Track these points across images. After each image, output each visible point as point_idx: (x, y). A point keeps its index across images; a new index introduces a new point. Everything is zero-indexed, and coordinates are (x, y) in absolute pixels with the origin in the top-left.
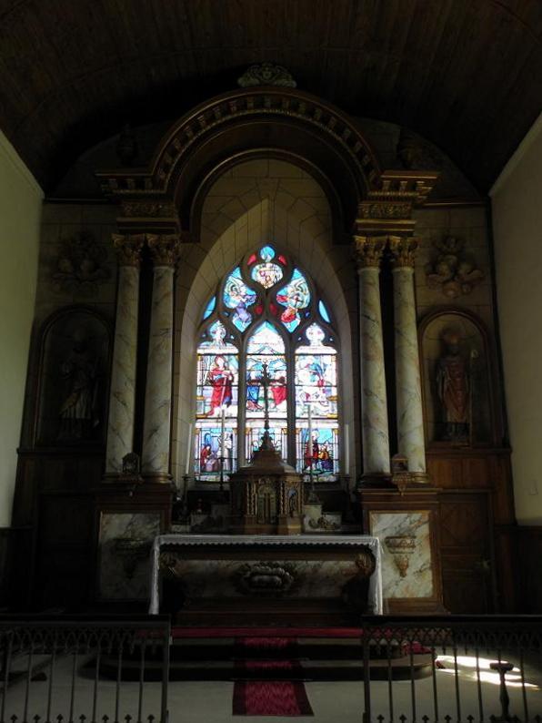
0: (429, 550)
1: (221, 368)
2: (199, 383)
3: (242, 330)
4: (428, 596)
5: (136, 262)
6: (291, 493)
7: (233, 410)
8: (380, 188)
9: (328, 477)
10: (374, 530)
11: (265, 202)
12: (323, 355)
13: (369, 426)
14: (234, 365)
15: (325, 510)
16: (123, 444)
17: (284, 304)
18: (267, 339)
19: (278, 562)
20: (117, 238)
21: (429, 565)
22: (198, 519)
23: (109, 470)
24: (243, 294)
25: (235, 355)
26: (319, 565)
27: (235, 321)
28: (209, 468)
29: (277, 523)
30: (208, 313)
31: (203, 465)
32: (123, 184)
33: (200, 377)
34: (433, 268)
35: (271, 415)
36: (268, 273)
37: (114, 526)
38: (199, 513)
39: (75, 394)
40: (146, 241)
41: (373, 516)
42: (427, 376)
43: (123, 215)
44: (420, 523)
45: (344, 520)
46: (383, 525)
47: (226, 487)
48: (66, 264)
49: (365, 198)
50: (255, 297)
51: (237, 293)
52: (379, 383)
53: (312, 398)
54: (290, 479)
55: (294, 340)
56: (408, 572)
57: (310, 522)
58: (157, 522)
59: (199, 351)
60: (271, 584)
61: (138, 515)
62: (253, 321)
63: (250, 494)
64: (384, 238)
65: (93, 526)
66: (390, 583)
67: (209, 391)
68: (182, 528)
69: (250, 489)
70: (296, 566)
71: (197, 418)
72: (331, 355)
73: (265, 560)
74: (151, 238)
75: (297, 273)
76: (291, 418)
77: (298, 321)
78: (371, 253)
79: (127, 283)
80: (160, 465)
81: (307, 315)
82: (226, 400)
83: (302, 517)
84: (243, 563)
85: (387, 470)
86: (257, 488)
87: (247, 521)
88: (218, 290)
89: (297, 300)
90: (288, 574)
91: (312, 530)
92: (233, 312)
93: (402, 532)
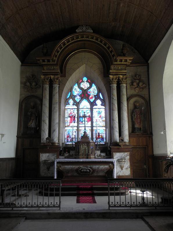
1: (72, 112)
2: (66, 117)
5: (48, 83)
7: (76, 124)
9: (102, 143)
10: (114, 157)
13: (113, 129)
14: (76, 111)
15: (101, 152)
16: (45, 135)
17: (90, 94)
18: (85, 104)
20: (42, 77)
21: (129, 167)
22: (67, 155)
23: (42, 141)
24: (78, 91)
25: (76, 109)
27: (76, 99)
28: (69, 141)
29: (88, 156)
30: (68, 97)
31: (67, 139)
32: (44, 61)
33: (66, 115)
34: (132, 84)
36: (85, 85)
37: (44, 157)
40: (51, 77)
41: (114, 154)
42: (130, 115)
45: (106, 155)
46: (117, 156)
47: (74, 146)
48: (28, 84)
49: (112, 64)
51: (76, 91)
52: (116, 117)
54: (91, 144)
55: (93, 104)
56: (123, 168)
58: (55, 156)
59: (66, 108)
60: (86, 172)
61: (50, 154)
62: (81, 99)
65: (38, 157)
67: (69, 119)
74: (52, 77)
75: (93, 84)
76: (92, 126)
77: (94, 99)
79: (46, 89)
80: (56, 140)
83: (95, 154)
84: (79, 166)
85: (118, 141)
87: (80, 155)
88: (71, 90)
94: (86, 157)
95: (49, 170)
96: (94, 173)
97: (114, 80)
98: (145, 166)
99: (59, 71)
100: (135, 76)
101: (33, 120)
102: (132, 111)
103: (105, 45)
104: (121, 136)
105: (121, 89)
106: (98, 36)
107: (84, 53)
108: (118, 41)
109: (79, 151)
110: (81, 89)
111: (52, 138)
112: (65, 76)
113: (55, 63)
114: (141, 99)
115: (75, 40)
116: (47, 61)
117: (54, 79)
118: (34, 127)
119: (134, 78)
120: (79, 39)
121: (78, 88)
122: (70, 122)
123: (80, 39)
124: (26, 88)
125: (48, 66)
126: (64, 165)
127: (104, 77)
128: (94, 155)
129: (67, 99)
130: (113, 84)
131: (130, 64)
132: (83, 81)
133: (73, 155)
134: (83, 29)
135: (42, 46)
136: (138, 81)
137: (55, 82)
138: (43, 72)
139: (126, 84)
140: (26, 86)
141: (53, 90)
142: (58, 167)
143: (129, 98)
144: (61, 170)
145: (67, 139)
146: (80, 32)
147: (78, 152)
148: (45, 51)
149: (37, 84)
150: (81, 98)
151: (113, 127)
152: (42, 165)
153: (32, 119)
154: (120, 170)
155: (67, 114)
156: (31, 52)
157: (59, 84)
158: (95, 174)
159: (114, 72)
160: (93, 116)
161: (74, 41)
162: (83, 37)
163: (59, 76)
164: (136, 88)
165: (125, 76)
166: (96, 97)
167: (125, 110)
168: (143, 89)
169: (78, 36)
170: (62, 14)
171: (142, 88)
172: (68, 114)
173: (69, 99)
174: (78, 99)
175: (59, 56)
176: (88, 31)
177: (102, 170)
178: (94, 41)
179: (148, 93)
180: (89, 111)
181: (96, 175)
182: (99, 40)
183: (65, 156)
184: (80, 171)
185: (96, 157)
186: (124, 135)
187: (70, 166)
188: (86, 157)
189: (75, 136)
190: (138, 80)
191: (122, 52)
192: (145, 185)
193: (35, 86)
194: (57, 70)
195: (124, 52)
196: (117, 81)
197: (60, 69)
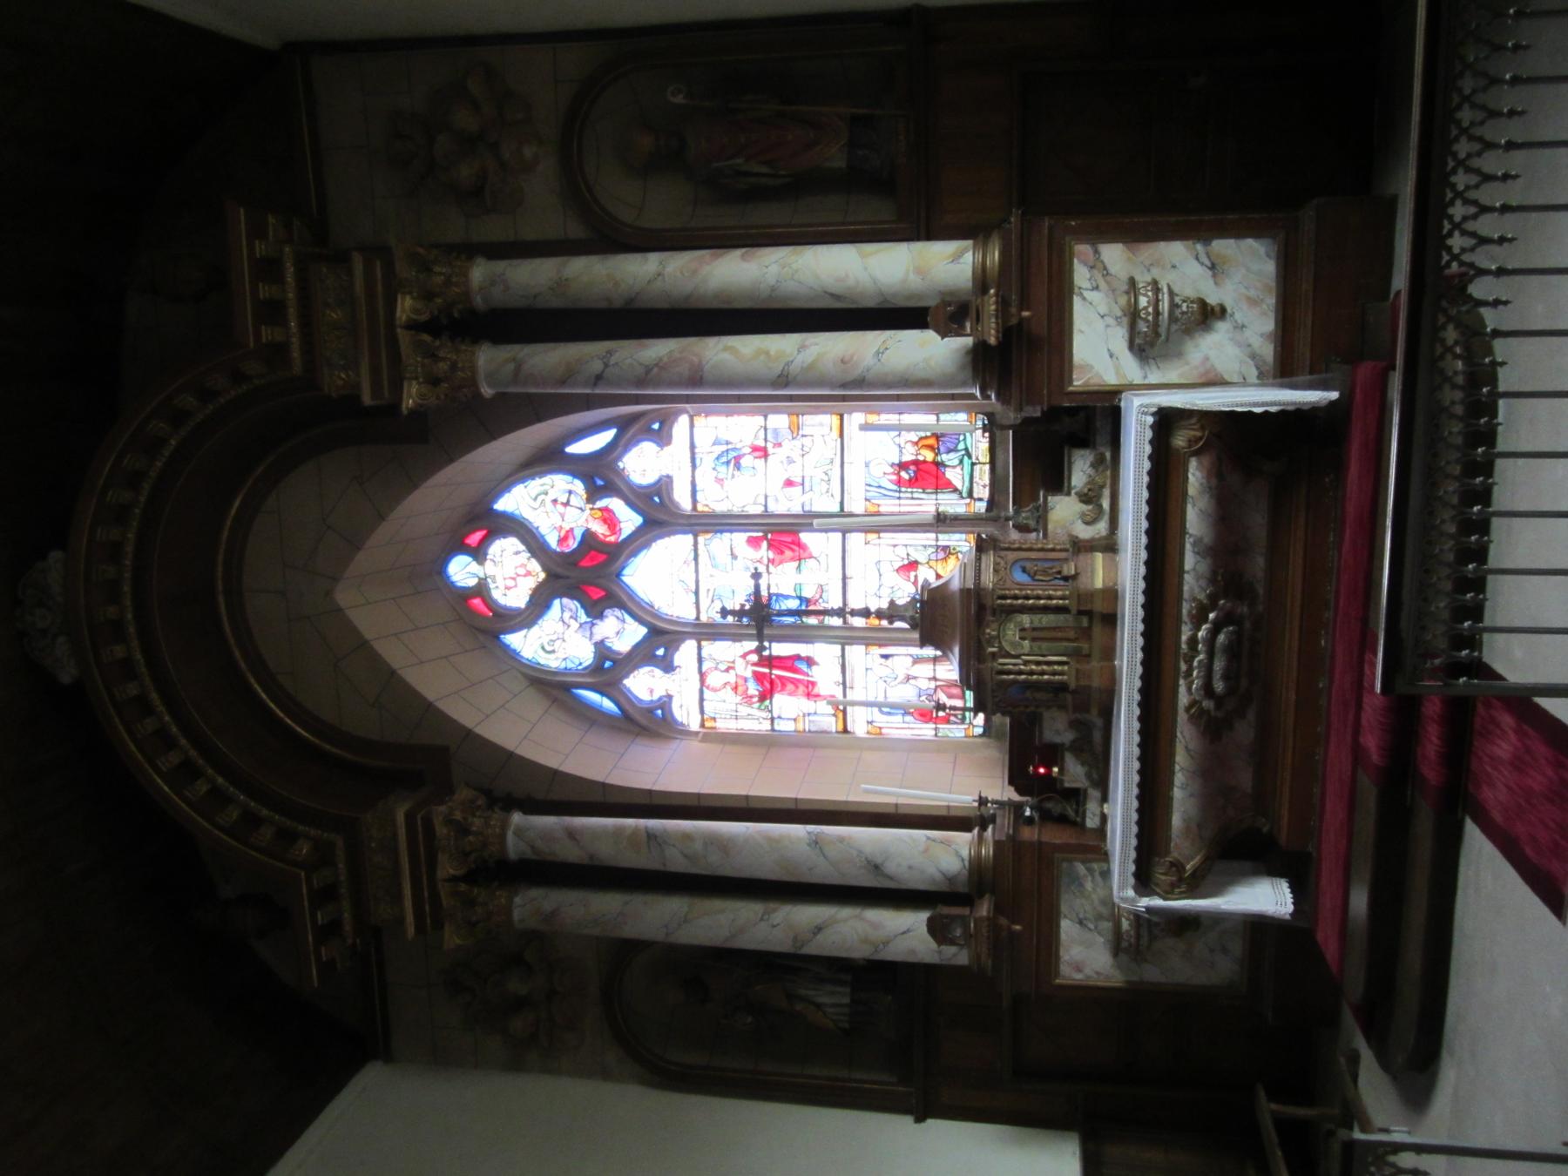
0: (1162, 244)
1: (731, 677)
2: (766, 726)
3: (643, 631)
4: (1276, 249)
6: (1020, 577)
7: (824, 653)
8: (278, 351)
12: (693, 447)
17: (578, 534)
19: (1184, 638)
21: (1199, 247)
24: (560, 627)
25: (700, 648)
26: (1194, 545)
29: (1089, 614)
30: (608, 704)
33: (753, 721)
35: (836, 603)
38: (1061, 770)
39: (799, 1007)
40: (454, 879)
41: (1078, 382)
43: (401, 920)
44: (1097, 265)
45: (1084, 442)
50: (566, 601)
52: (759, 352)
54: (988, 579)
56: (1212, 300)
57: (1087, 523)
58: (1081, 868)
59: (694, 725)
60: (1233, 651)
61: (1064, 908)
62: (622, 606)
63: (1020, 673)
64: (404, 337)
65: (1090, 997)
66: (1239, 345)
68: (1092, 807)
69: (1009, 673)
70: (1194, 599)
71: (845, 731)
72: (692, 426)
73: (1177, 669)
74: (447, 868)
75: (504, 504)
77: (616, 504)
78: (443, 366)
81: (600, 482)
82: (803, 667)
84: (1182, 717)
85: (968, 341)
86: (1008, 655)
87: (1083, 682)
89: (567, 504)
90: (1212, 616)
91: (1106, 517)
92: (602, 650)
93: (1119, 313)
94: (1098, 631)
109: (1048, 682)
110: (539, 603)
118: (848, 990)
121: (535, 629)
122: (808, 695)
123: (135, 643)
126: (1169, 839)
132: (481, 590)
133: (1074, 724)
142: (1181, 880)
152: (1152, 973)
154: (1222, 328)
160: (759, 510)
167: (695, 272)
172: (744, 710)
173: (622, 700)
174: (622, 633)
180: (717, 545)
186: (915, 283)
188: (1098, 631)
189: (917, 660)
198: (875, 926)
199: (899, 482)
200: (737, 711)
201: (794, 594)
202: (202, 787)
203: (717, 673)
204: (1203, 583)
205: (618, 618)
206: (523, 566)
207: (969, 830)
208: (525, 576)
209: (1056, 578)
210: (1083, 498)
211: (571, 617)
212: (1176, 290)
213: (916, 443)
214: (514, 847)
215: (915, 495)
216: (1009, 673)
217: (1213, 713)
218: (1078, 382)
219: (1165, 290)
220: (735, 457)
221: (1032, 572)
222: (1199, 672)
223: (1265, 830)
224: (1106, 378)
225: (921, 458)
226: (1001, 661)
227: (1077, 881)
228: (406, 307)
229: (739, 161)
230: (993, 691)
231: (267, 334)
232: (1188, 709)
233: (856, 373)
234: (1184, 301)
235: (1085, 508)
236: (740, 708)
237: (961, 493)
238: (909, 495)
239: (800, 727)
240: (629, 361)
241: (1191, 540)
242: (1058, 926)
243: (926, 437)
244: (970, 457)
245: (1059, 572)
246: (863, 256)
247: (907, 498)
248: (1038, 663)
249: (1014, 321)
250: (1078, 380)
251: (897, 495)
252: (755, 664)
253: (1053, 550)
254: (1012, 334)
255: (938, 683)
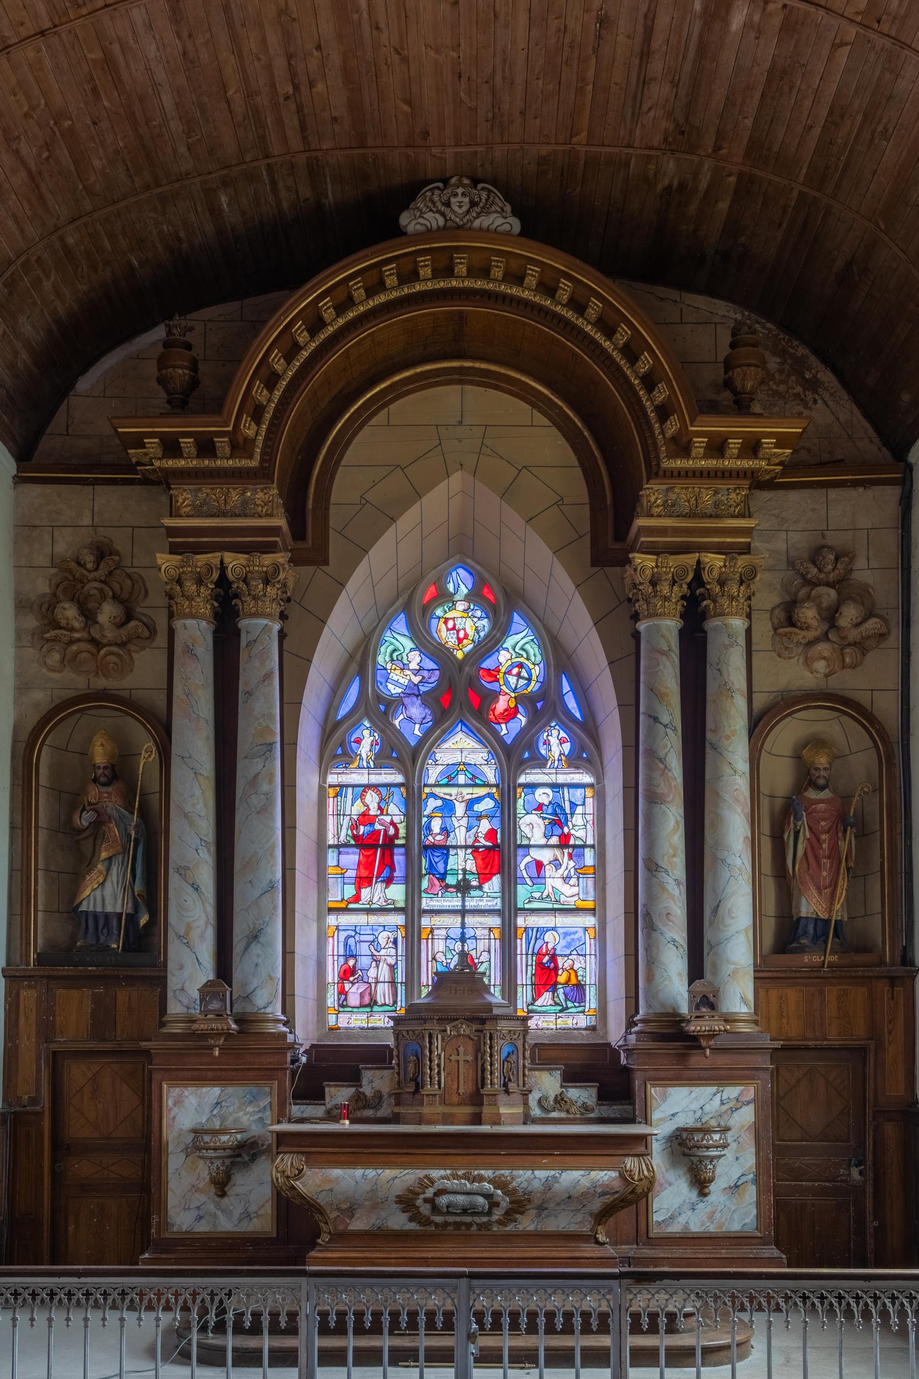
5: (206, 609)
6: (506, 1050)
8: (682, 447)
10: (656, 1115)
11: (457, 479)
14: (395, 812)
20: (166, 561)
21: (751, 1176)
22: (338, 1095)
23: (174, 1008)
26: (554, 1177)
28: (354, 1000)
32: (171, 447)
40: (223, 568)
41: (654, 1092)
42: (766, 827)
44: (739, 1103)
45: (603, 1097)
48: (69, 612)
49: (655, 473)
53: (549, 871)
56: (713, 1187)
57: (539, 1101)
58: (265, 1102)
61: (230, 1090)
62: (437, 723)
64: (690, 560)
69: (431, 1043)
70: (513, 1179)
74: (234, 562)
82: (386, 873)
83: (525, 1094)
84: (421, 1173)
85: (684, 1009)
91: (544, 1115)
93: (704, 1120)
94: (468, 1110)
95: (223, 1194)
96: (522, 1213)
97: (665, 589)
98: (855, 1172)
99: (280, 522)
100: (814, 563)
101: (110, 859)
102: (779, 802)
103: (610, 333)
104: (701, 977)
105: (711, 656)
106: (557, 261)
107: (458, 387)
108: (700, 301)
109: (424, 1074)
111: (245, 984)
112: (319, 557)
113: (254, 463)
114: (845, 718)
115: (395, 294)
116: (193, 451)
117: (245, 581)
119: (803, 576)
120: (305, 354)
124: (55, 640)
125: (206, 489)
127: (594, 564)
128: (517, 1097)
129: (338, 724)
130: (722, 614)
131: (783, 474)
133: (379, 1096)
134: (448, 204)
135: (158, 333)
136: (829, 595)
137: (255, 598)
138: (172, 532)
139: (749, 616)
140: (60, 628)
141: (243, 655)
143: (760, 718)
144: (300, 1196)
145: (342, 992)
146: (429, 231)
147: (414, 1079)
148: (181, 373)
149: (129, 616)
150: (433, 713)
151: (648, 915)
152: (175, 1162)
153: (104, 855)
154: (693, 1195)
155: (339, 827)
156: (83, 384)
157: (283, 616)
158: (527, 1223)
159: (663, 531)
161: (382, 298)
162: (448, 272)
163: (281, 558)
164: (810, 644)
165: (742, 561)
166: (539, 705)
168: (864, 652)
169: (416, 263)
170: (296, 87)
171: (855, 644)
172: (346, 822)
175: (276, 410)
176: (485, 221)
177: (573, 1200)
178: (526, 303)
179: (893, 680)
181: (531, 1228)
182: (565, 290)
183: (329, 1102)
184: (426, 1200)
185: (536, 1112)
186: (727, 969)
187: (359, 1172)
188: (468, 1110)
190: (828, 584)
191: (728, 384)
192: (866, 1314)
193: (123, 624)
194: (270, 515)
195: (738, 384)
196: (683, 597)
197: (285, 505)
198: (202, 936)
199: (540, 955)
200: (344, 815)
201: (449, 868)
202: (302, 338)
203: (377, 799)
204: (524, 1185)
205: (424, 718)
206: (466, 636)
207: (284, 1012)
208: (458, 638)
209: (505, 1078)
210: (559, 1098)
211: (423, 677)
212: (721, 1160)
213: (572, 968)
214: (251, 626)
215: (530, 968)
216: (431, 1043)
217: (422, 1196)
218: (654, 1092)
219: (723, 1153)
220: (560, 820)
221: (509, 1059)
222: (457, 1184)
223: (319, 1241)
224: (656, 1112)
225: (560, 972)
226: (440, 1036)
227: (254, 1099)
228: (715, 561)
229: (808, 835)
230: (413, 1031)
231: (700, 442)
232: (427, 1177)
233: (659, 924)
234: (714, 1166)
235: (551, 1099)
236: (347, 819)
237: (532, 1004)
238: (530, 963)
239: (330, 870)
240: (669, 745)
241: (557, 1175)
242: (215, 1085)
243: (577, 976)
244: (561, 1011)
245: (510, 1080)
246: (746, 930)
247: (527, 961)
248: (439, 1065)
249: (704, 1043)
250: (655, 1092)
251: (530, 952)
252: (385, 831)
253: (524, 1075)
254: (693, 1042)
255: (373, 985)
